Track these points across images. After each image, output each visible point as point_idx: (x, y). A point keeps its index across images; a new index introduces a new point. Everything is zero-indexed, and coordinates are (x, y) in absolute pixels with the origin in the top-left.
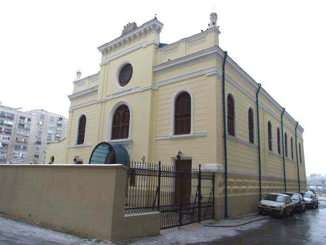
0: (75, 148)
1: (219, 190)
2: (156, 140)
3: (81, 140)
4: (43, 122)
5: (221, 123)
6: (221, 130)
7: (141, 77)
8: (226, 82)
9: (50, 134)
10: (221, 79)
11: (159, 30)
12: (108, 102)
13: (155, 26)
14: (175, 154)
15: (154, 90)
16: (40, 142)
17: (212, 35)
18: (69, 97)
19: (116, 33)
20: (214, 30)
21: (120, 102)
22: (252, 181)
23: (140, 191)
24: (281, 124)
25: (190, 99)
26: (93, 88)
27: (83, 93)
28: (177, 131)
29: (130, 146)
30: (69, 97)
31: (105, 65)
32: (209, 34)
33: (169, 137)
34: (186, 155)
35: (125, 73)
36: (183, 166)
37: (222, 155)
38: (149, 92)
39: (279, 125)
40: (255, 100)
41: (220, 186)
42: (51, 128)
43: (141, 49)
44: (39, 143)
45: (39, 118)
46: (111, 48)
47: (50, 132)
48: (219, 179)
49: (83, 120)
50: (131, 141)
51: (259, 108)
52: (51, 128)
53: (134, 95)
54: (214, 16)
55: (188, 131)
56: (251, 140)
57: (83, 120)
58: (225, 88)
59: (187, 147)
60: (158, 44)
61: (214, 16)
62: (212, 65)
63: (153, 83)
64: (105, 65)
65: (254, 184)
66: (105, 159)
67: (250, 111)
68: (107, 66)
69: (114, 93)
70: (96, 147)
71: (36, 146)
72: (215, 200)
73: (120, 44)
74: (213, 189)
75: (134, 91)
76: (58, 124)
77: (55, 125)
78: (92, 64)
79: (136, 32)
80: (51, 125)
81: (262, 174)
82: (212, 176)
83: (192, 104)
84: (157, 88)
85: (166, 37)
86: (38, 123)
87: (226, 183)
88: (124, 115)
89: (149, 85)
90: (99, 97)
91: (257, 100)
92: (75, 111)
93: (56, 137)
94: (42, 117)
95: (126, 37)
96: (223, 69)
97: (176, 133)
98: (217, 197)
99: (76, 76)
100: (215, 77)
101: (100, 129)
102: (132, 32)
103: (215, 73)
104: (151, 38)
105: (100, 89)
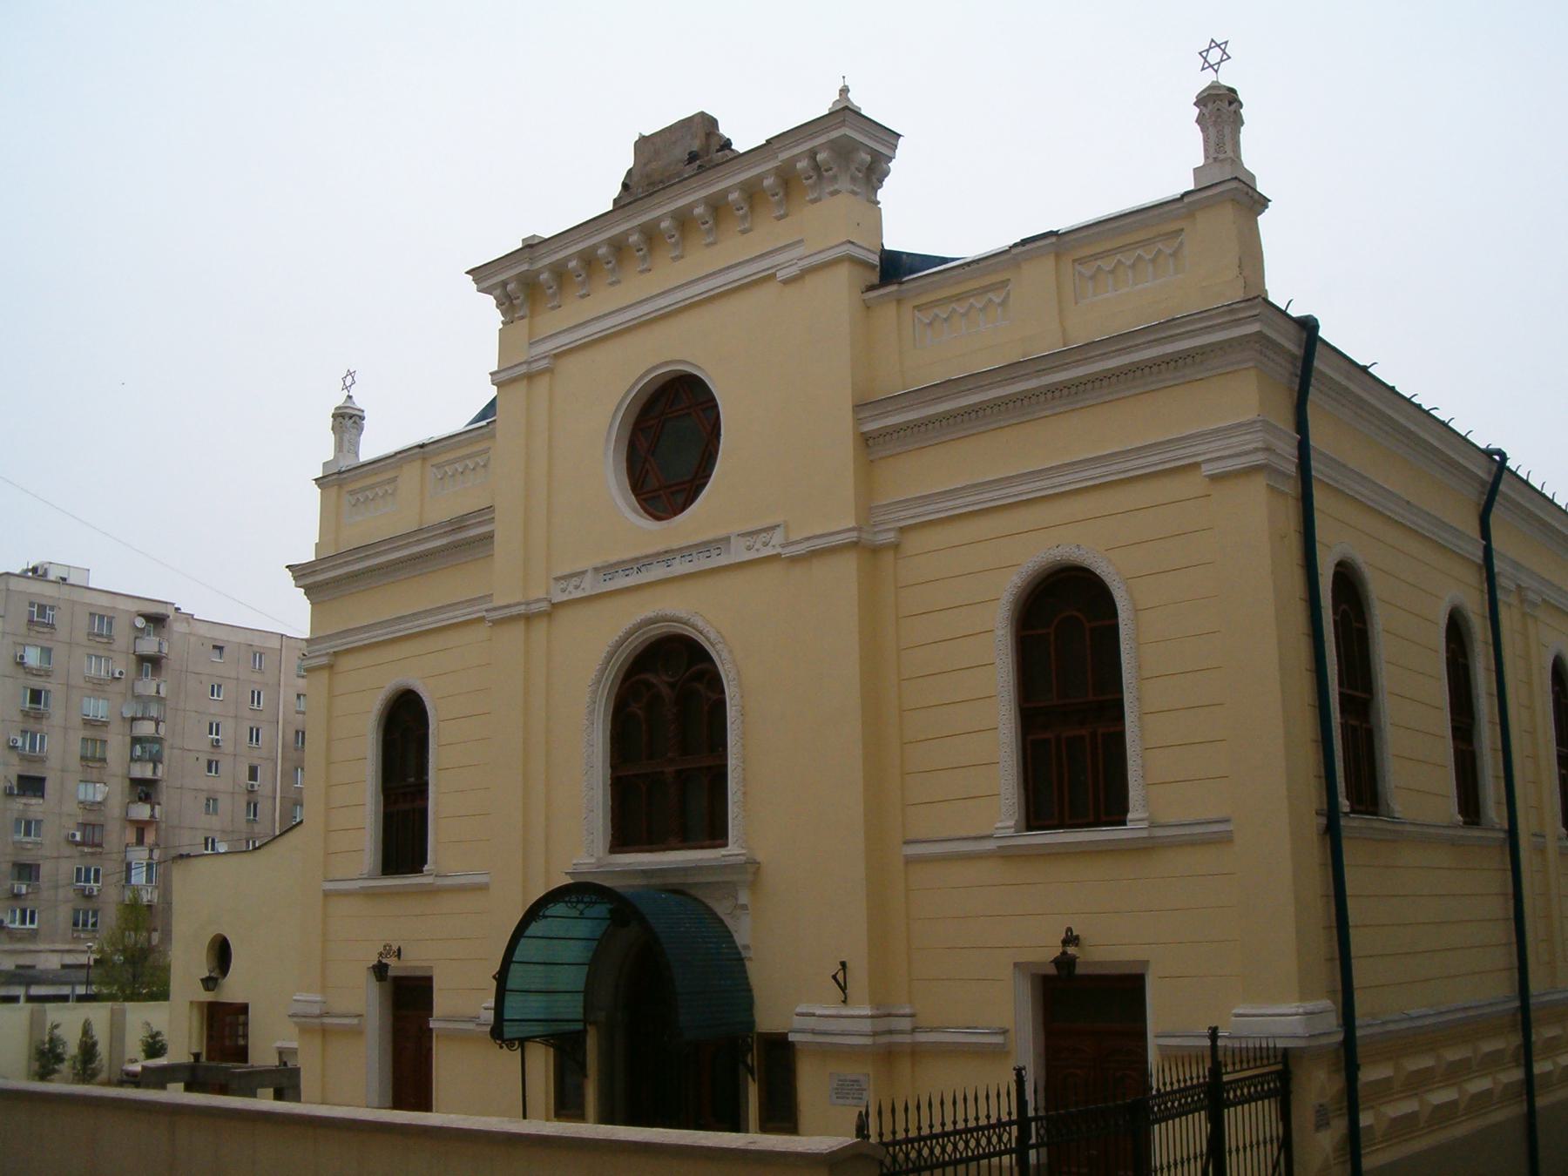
2: (909, 861)
3: (403, 843)
4: (47, 652)
5: (1309, 758)
6: (1312, 797)
7: (780, 455)
8: (1319, 498)
9: (89, 723)
10: (1292, 488)
11: (874, 171)
13: (846, 150)
14: (1046, 951)
15: (876, 550)
16: (42, 780)
17: (1225, 218)
18: (300, 572)
19: (583, 186)
20: (1228, 195)
26: (458, 524)
28: (1042, 807)
29: (744, 898)
30: (300, 572)
31: (530, 377)
33: (990, 845)
34: (1106, 948)
35: (671, 440)
36: (1087, 1008)
37: (1322, 943)
38: (847, 567)
40: (1478, 555)
41: (1322, 1122)
42: (98, 686)
43: (768, 292)
44: (31, 785)
45: (23, 629)
46: (560, 273)
47: (97, 708)
48: (1317, 1086)
49: (405, 723)
50: (751, 869)
51: (1500, 595)
52: (98, 686)
54: (1220, 110)
55: (1112, 809)
56: (1470, 806)
57: (405, 723)
58: (1320, 534)
60: (875, 259)
61: (1220, 110)
62: (1239, 406)
63: (867, 509)
64: (530, 377)
65: (1491, 1062)
66: (581, 997)
67: (1456, 629)
68: (542, 384)
69: (613, 559)
70: (534, 913)
71: (19, 804)
73: (619, 247)
74: (1286, 1144)
76: (142, 659)
77: (122, 665)
79: (726, 182)
80: (97, 669)
81: (1534, 987)
82: (1277, 1074)
84: (890, 537)
86: (20, 663)
87: (1352, 1101)
89: (841, 520)
90: (504, 579)
92: (345, 663)
93: (136, 740)
94: (40, 617)
95: (661, 210)
96: (1301, 426)
97: (1037, 815)
99: (330, 439)
101: (531, 802)
103: (1259, 458)
104: (820, 224)
105: (505, 531)
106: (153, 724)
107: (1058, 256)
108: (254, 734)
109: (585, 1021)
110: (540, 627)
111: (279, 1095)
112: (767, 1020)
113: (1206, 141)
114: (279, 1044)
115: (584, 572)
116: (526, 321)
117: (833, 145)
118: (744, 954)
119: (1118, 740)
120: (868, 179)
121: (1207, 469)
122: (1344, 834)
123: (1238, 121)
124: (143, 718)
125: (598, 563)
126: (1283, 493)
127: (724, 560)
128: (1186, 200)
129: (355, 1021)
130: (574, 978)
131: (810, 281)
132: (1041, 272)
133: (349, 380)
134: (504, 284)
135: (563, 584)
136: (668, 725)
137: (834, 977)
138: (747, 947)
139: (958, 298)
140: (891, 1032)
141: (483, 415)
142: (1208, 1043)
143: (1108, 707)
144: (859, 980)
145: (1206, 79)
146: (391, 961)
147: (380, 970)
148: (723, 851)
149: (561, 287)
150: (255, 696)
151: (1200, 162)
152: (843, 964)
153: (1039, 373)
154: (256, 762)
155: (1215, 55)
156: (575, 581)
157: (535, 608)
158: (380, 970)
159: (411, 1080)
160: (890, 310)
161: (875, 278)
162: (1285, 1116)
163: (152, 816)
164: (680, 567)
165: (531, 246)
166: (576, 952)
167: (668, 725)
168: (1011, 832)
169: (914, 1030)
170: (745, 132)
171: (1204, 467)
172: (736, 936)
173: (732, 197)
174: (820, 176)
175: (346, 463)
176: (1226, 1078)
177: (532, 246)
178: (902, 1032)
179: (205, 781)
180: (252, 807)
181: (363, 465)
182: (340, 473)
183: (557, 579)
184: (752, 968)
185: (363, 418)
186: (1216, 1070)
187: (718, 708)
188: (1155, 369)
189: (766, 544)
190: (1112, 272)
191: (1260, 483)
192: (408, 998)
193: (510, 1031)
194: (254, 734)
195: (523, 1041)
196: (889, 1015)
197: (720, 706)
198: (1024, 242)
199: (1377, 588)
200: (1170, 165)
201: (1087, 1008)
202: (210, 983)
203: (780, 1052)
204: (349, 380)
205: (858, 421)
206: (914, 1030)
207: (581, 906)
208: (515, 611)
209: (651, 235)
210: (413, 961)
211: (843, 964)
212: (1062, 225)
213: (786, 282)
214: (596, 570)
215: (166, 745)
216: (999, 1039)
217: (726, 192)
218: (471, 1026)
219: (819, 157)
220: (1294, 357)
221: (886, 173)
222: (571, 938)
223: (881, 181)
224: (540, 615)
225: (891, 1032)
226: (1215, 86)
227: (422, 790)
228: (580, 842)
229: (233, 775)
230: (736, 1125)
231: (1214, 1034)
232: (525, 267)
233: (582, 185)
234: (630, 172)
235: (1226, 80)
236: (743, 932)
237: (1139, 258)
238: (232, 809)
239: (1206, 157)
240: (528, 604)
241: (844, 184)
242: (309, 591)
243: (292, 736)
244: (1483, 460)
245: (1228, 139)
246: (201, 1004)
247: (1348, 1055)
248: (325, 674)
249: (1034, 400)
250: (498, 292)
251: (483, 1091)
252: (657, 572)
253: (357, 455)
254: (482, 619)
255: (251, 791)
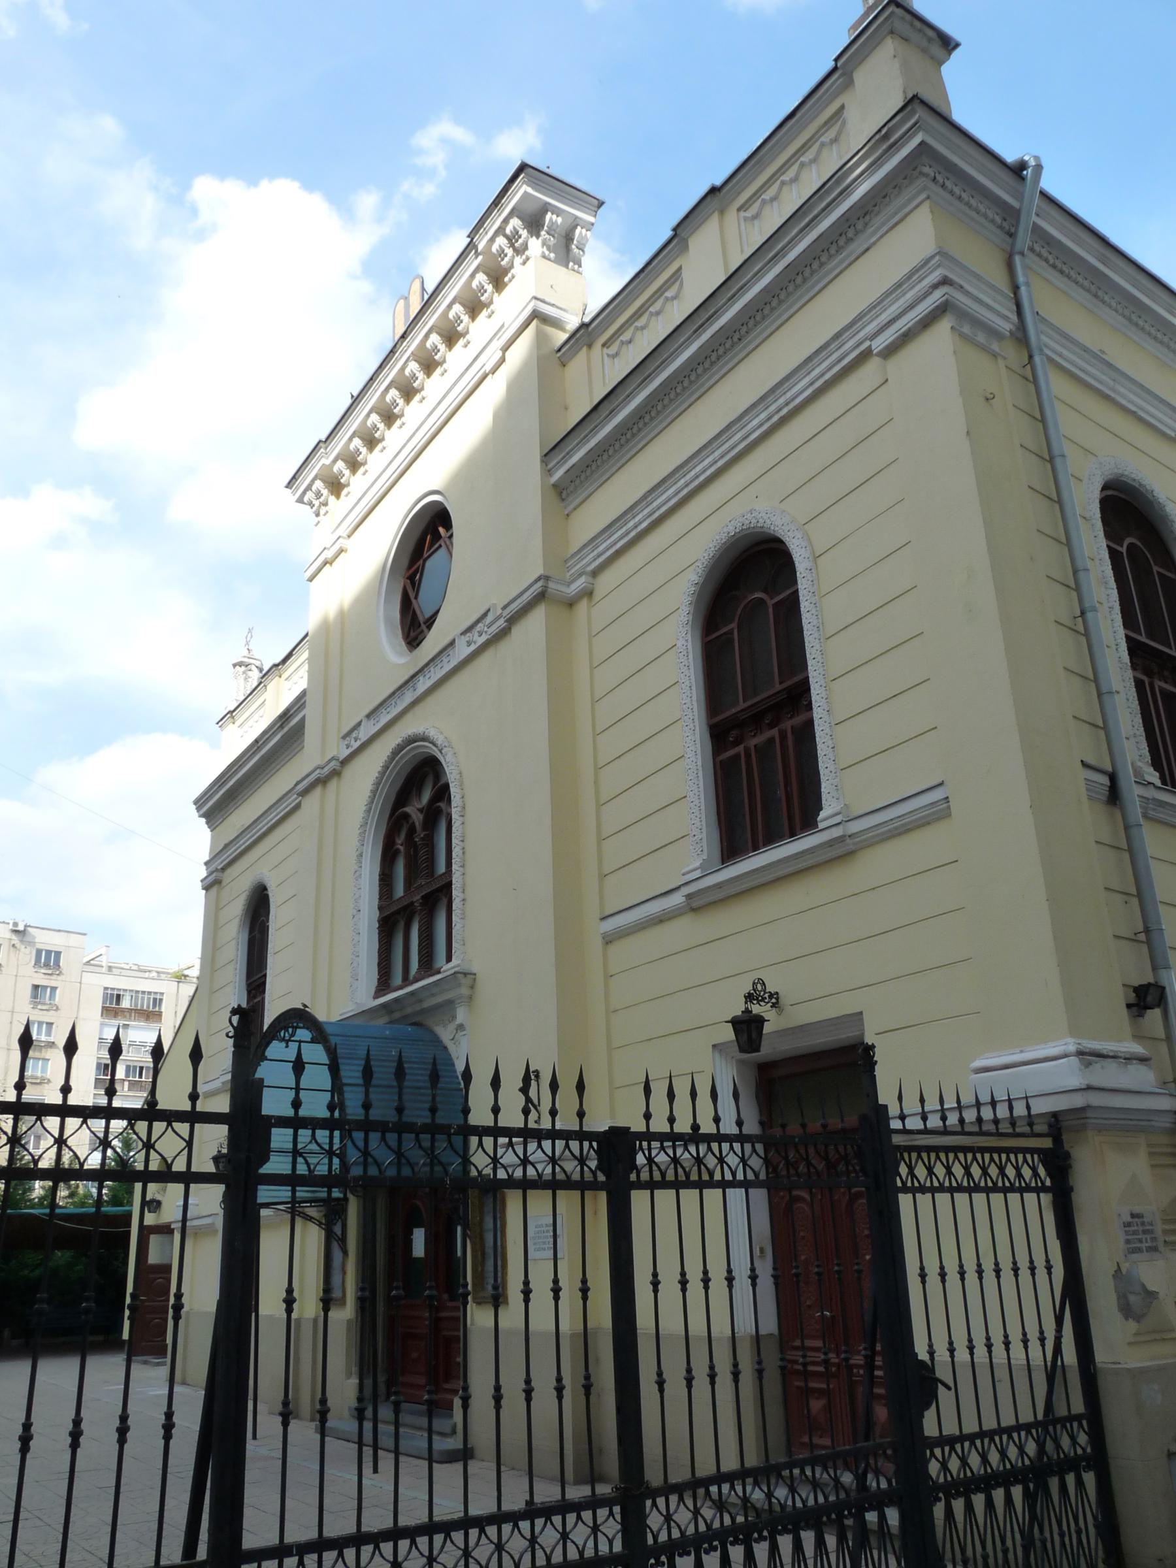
22: (881, 1413)
23: (387, 1441)
33: (678, 899)
34: (809, 1005)
53: (511, 598)
59: (826, 948)
72: (1106, 1386)
83: (804, 606)
84: (581, 582)
98: (1134, 1359)
100: (944, 326)
103: (937, 296)
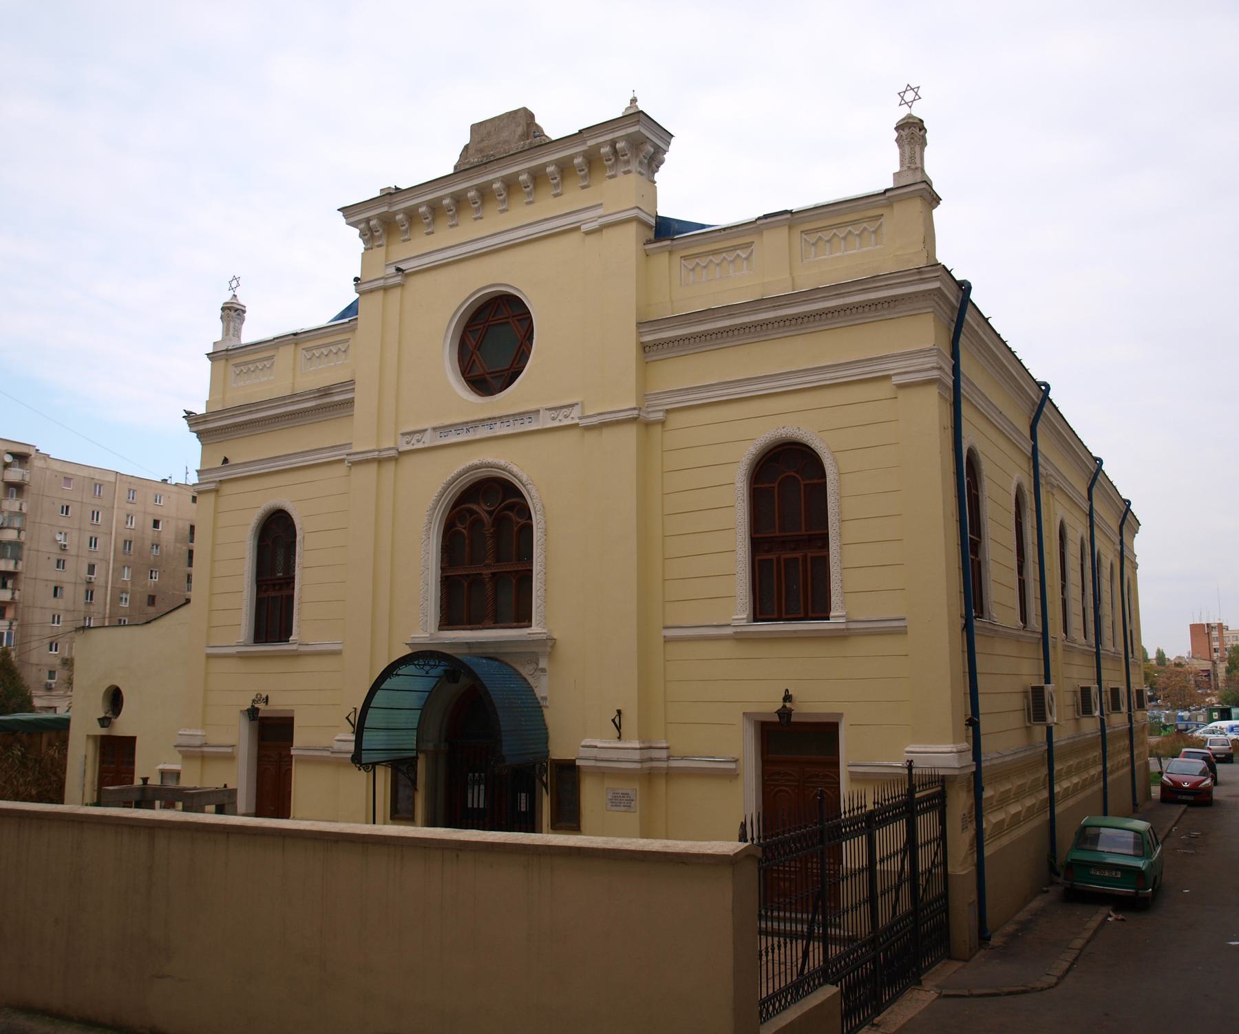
0: (242, 656)
1: (960, 841)
2: (667, 640)
3: (273, 615)
10: (949, 396)
11: (653, 161)
12: (409, 463)
13: (635, 142)
14: (770, 705)
15: (648, 425)
17: (917, 205)
19: (433, 156)
20: (915, 193)
21: (476, 467)
24: (1026, 466)
25: (823, 475)
26: (326, 392)
27: (265, 401)
29: (543, 664)
32: (896, 206)
33: (729, 631)
35: (494, 339)
36: (796, 748)
39: (1019, 474)
43: (575, 238)
49: (276, 535)
50: (548, 645)
54: (912, 133)
55: (820, 610)
57: (276, 535)
60: (653, 222)
61: (912, 133)
62: (921, 335)
63: (644, 395)
66: (415, 733)
67: (1019, 489)
73: (459, 201)
75: (545, 422)
76: (9, 485)
78: (309, 279)
84: (660, 416)
85: (680, 192)
88: (500, 521)
89: (626, 402)
90: (360, 433)
91: (956, 384)
92: (227, 489)
95: (494, 176)
96: (955, 355)
97: (759, 614)
99: (219, 325)
101: (376, 593)
102: (508, 155)
104: (614, 193)
105: (363, 399)
106: (16, 532)
107: (790, 228)
108: (93, 542)
109: (417, 750)
110: (390, 468)
111: (220, 810)
112: (559, 751)
113: (902, 155)
114: (161, 767)
115: (426, 430)
116: (384, 248)
117: (628, 138)
118: (542, 703)
119: (825, 561)
120: (649, 165)
121: (897, 380)
122: (976, 631)
123: (924, 143)
124: (8, 528)
125: (436, 424)
126: (946, 400)
127: (534, 427)
128: (888, 194)
129: (229, 750)
130: (413, 719)
131: (607, 233)
132: (777, 238)
133: (234, 284)
134: (368, 220)
135: (408, 438)
136: (487, 539)
137: (613, 721)
138: (545, 698)
139: (715, 252)
140: (651, 760)
141: (342, 315)
142: (906, 771)
143: (816, 539)
144: (631, 722)
145: (903, 112)
146: (261, 706)
147: (252, 713)
148: (527, 631)
149: (458, 210)
150: (95, 515)
151: (897, 169)
152: (619, 712)
153: (775, 308)
154: (93, 562)
155: (909, 96)
156: (417, 436)
157: (385, 454)
158: (252, 713)
159: (273, 793)
160: (664, 259)
161: (651, 235)
162: (943, 821)
163: (13, 598)
164: (500, 430)
165: (390, 194)
166: (413, 700)
167: (487, 539)
168: (744, 622)
169: (668, 758)
170: (555, 125)
171: (894, 378)
172: (536, 690)
173: (576, 161)
174: (617, 159)
175: (232, 344)
176: (917, 795)
177: (392, 194)
178: (658, 760)
179: (55, 575)
180: (90, 594)
181: (247, 346)
182: (227, 350)
183: (403, 434)
184: (547, 713)
185: (244, 312)
186: (911, 790)
187: (526, 531)
188: (860, 310)
189: (566, 417)
190: (829, 241)
191: (933, 391)
192: (272, 734)
193: (366, 758)
194: (93, 542)
195: (374, 764)
196: (651, 748)
197: (527, 529)
198: (766, 217)
199: (986, 468)
200: (878, 169)
201: (796, 748)
202: (104, 722)
203: (568, 773)
204: (234, 284)
205: (640, 334)
206: (668, 758)
207: (427, 668)
208: (370, 456)
209: (485, 193)
210: (278, 704)
211: (619, 712)
212: (795, 206)
213: (588, 233)
214: (434, 429)
215: (26, 547)
216: (732, 766)
217: (545, 165)
218: (328, 754)
219: (618, 146)
220: (953, 307)
221: (662, 162)
222: (411, 689)
223: (658, 167)
224: (389, 459)
225: (651, 760)
226: (910, 116)
227: (289, 581)
228: (417, 621)
229: (76, 570)
230: (531, 825)
231: (910, 767)
232: (385, 209)
233: (429, 154)
234: (466, 147)
235: (917, 111)
236: (542, 688)
237: (865, 229)
238: (73, 594)
239: (902, 166)
240: (380, 451)
241: (634, 166)
242: (200, 435)
243: (121, 544)
244: (1036, 388)
245: (918, 155)
246: (95, 737)
247: (977, 782)
248: (212, 497)
249: (770, 326)
250: (362, 226)
251: (335, 801)
252: (483, 432)
253: (239, 337)
254: (342, 461)
255: (89, 582)
